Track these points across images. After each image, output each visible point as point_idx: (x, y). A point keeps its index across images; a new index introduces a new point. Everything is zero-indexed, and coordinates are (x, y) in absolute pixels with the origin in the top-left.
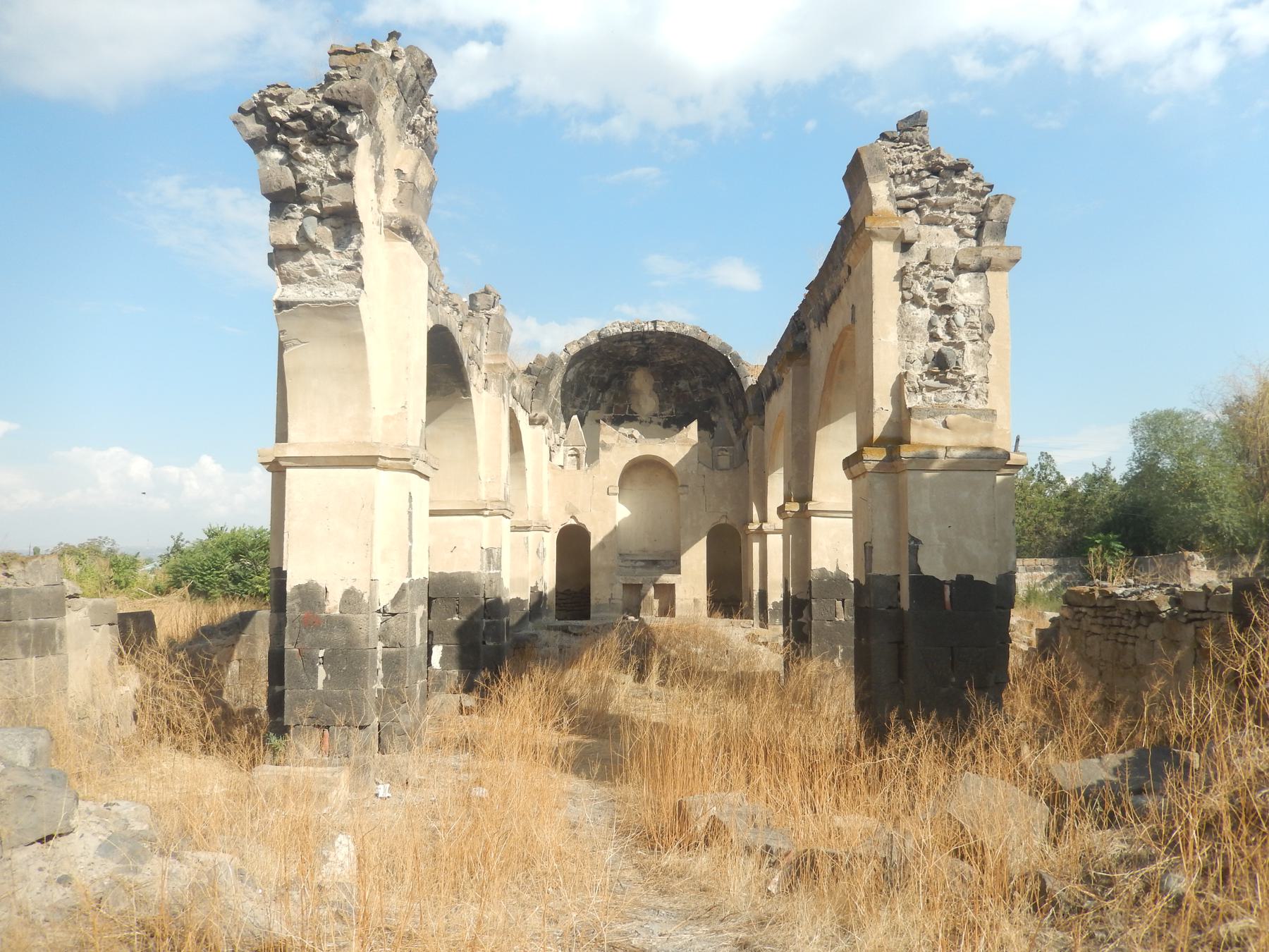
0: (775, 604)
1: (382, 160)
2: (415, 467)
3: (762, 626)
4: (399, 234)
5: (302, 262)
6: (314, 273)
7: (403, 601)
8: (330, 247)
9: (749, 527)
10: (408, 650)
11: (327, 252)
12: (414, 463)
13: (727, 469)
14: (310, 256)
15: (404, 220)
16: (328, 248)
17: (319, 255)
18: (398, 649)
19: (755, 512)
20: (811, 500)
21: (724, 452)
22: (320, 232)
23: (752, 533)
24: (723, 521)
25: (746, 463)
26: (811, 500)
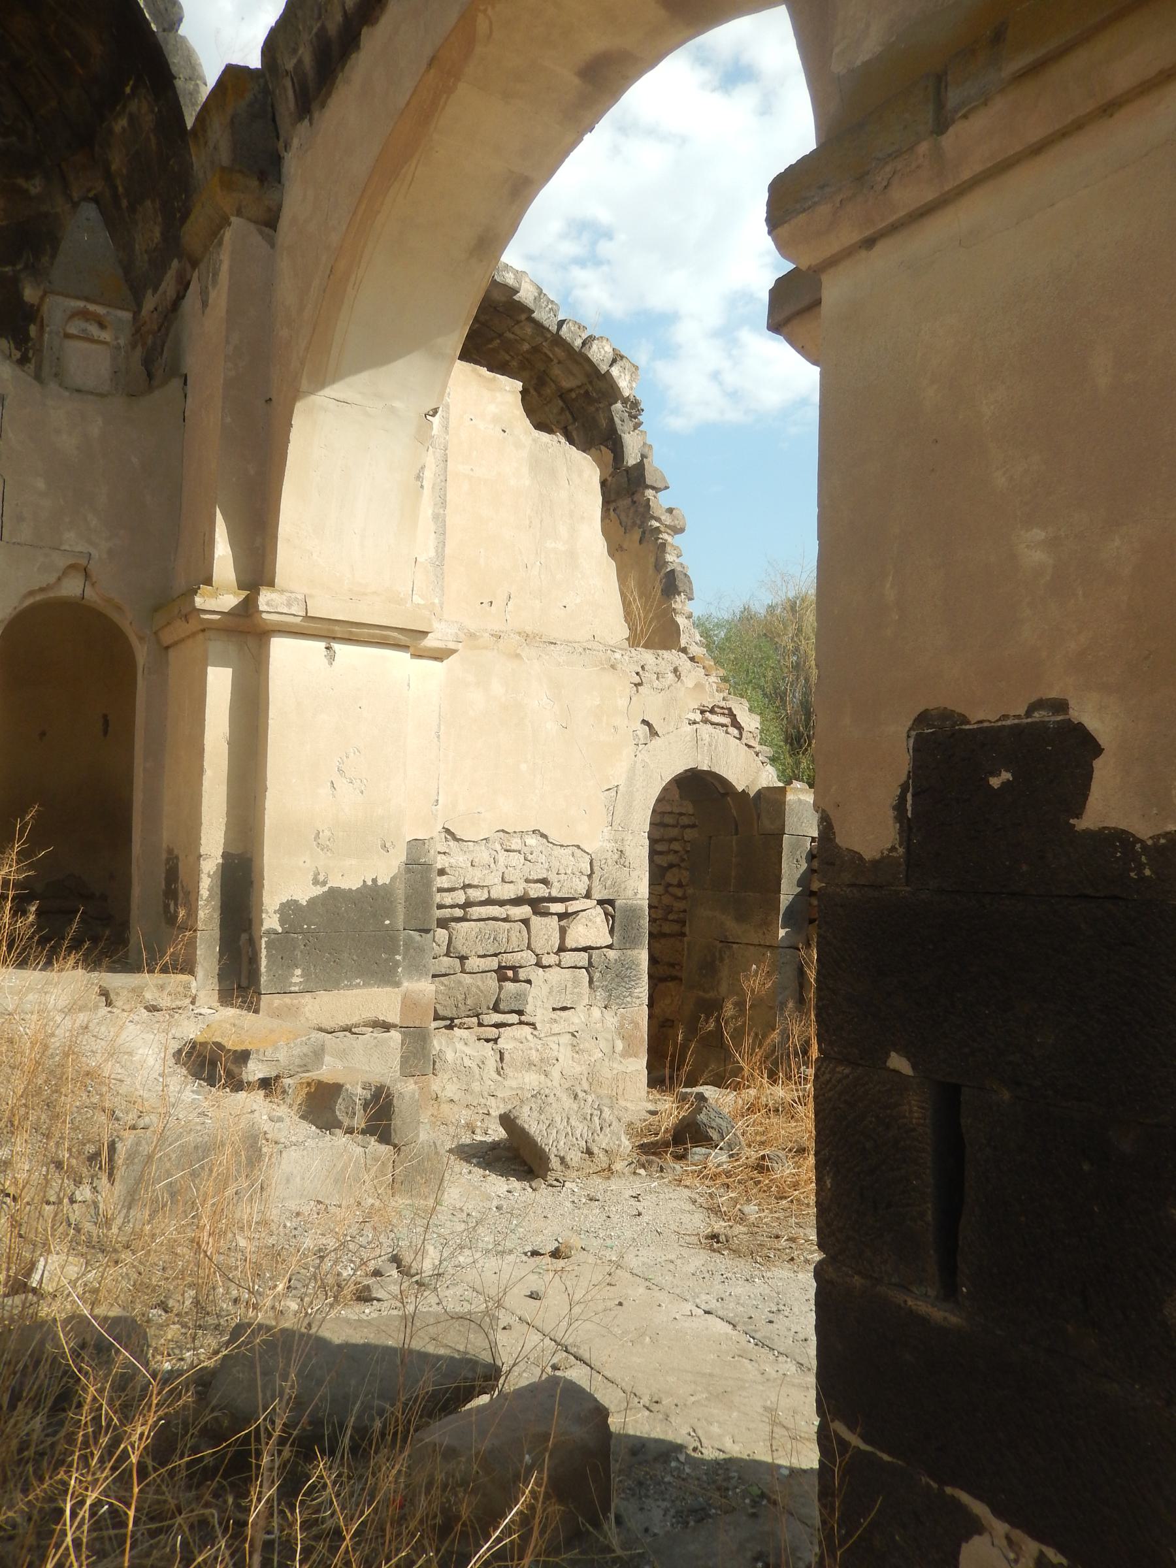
0: (289, 910)
3: (226, 998)
9: (199, 602)
13: (102, 395)
19: (223, 550)
20: (271, 584)
21: (94, 330)
23: (207, 628)
24: (72, 588)
25: (176, 383)
26: (271, 584)
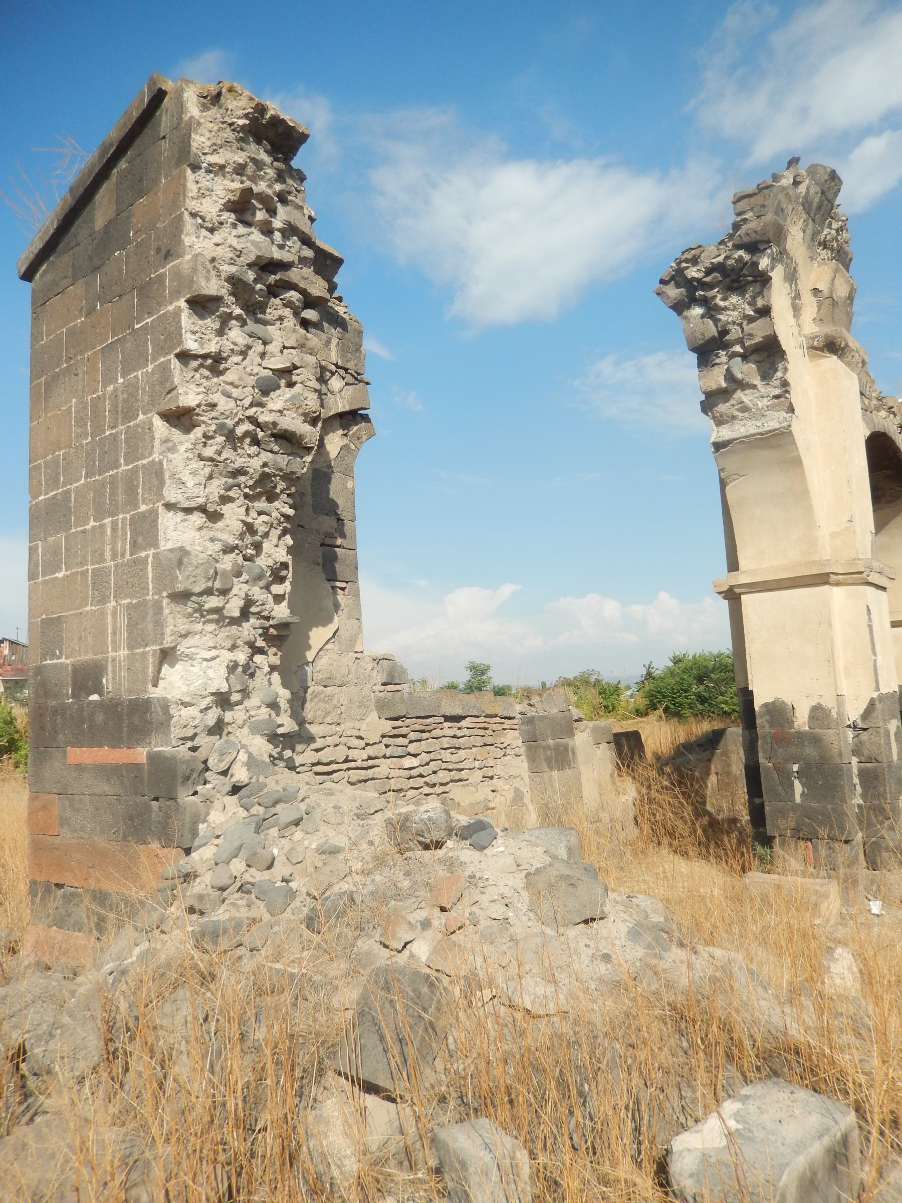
2: (870, 579)
4: (823, 351)
5: (732, 402)
6: (745, 409)
7: (873, 715)
8: (757, 381)
10: (885, 765)
11: (754, 387)
12: (868, 576)
14: (739, 394)
15: (826, 336)
16: (755, 383)
17: (747, 392)
18: (874, 765)
22: (746, 370)
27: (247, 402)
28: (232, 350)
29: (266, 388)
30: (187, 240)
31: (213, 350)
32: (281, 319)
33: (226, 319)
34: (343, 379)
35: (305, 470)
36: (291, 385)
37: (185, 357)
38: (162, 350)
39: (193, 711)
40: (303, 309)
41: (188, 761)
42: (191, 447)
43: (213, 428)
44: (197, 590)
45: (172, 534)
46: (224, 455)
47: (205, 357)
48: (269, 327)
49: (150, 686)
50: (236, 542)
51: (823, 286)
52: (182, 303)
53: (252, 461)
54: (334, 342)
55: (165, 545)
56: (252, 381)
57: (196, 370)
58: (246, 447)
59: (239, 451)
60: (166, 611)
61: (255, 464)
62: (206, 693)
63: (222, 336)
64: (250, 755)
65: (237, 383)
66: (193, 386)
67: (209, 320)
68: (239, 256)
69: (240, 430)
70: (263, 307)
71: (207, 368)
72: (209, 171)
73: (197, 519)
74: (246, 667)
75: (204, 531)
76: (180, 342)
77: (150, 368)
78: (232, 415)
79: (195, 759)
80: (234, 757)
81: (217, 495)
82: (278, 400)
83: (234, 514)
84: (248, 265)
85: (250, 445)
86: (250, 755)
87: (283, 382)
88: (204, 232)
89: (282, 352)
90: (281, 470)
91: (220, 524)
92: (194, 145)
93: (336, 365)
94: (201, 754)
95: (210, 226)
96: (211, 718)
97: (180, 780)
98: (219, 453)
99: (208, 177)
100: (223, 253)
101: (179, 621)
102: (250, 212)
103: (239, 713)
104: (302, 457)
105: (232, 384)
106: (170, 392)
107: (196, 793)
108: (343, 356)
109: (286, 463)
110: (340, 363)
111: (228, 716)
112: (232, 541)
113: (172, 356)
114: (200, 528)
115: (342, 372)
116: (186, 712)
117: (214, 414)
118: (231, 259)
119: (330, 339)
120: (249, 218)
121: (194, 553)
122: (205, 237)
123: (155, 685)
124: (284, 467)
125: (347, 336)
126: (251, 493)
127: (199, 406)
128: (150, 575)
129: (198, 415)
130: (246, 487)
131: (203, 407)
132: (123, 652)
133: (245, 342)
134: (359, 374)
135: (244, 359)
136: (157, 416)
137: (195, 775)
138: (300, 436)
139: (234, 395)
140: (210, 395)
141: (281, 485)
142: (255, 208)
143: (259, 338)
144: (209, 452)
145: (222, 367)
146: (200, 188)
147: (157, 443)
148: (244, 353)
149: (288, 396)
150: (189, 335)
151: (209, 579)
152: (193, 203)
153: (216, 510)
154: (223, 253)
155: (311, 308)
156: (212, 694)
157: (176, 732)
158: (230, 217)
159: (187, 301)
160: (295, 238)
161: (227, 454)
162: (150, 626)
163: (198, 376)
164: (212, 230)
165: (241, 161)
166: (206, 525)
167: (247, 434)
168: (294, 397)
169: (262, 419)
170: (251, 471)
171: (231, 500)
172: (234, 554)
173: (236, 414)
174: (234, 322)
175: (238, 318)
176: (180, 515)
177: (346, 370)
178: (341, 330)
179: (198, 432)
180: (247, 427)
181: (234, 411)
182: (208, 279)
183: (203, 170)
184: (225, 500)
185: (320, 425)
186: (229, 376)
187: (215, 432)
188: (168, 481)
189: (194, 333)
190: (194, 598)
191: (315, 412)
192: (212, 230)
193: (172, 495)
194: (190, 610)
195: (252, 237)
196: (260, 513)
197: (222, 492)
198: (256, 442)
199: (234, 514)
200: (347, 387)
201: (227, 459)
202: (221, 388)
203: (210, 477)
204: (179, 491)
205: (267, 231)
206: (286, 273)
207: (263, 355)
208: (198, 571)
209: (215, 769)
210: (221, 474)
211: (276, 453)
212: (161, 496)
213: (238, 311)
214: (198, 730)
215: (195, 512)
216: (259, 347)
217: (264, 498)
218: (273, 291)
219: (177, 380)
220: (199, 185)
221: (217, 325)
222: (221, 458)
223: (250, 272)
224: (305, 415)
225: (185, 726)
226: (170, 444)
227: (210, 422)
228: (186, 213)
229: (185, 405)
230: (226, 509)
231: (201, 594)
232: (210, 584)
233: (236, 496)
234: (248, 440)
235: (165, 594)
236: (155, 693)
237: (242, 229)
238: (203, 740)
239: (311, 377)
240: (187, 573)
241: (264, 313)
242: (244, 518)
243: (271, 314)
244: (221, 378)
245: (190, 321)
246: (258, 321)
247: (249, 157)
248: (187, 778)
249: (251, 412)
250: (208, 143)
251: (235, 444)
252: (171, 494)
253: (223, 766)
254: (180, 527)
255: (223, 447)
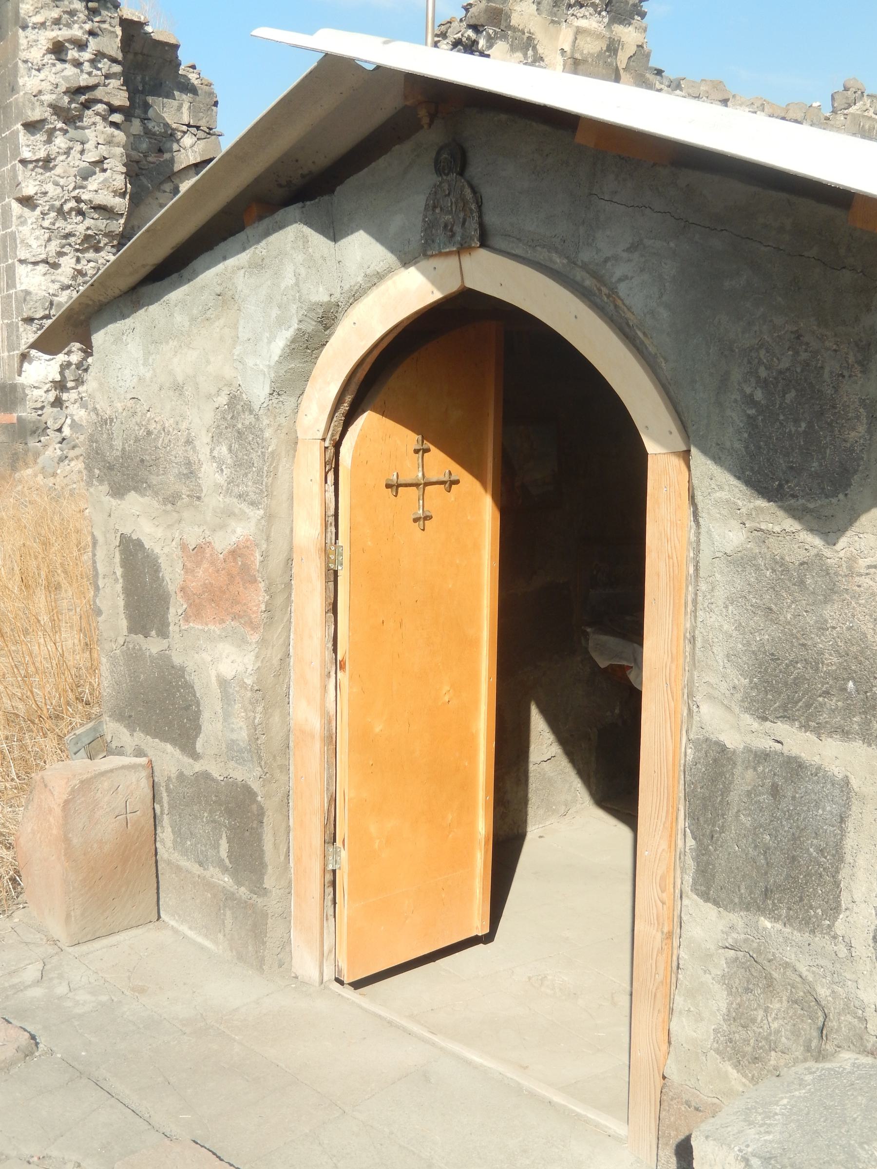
1: (534, 48)
27: (71, 187)
28: (58, 153)
29: (86, 175)
30: (21, 81)
31: (42, 156)
32: (94, 124)
33: (51, 133)
34: (195, 135)
35: (121, 229)
36: (104, 170)
37: (23, 162)
38: (14, 157)
39: (41, 392)
40: (110, 115)
41: (34, 422)
42: (35, 221)
43: (47, 208)
44: (38, 316)
45: (24, 280)
46: (57, 225)
47: (37, 161)
48: (86, 131)
49: (16, 376)
50: (70, 282)
51: (567, 48)
52: (19, 126)
53: (78, 226)
54: (186, 106)
55: (20, 287)
56: (74, 171)
57: (32, 170)
58: (74, 217)
59: (69, 220)
60: (21, 330)
61: (81, 229)
62: (47, 381)
63: (51, 143)
64: (73, 421)
65: (62, 175)
66: (31, 181)
67: (38, 135)
68: (56, 88)
69: (66, 208)
70: (80, 118)
71: (40, 167)
72: (34, 28)
73: (42, 268)
74: (79, 366)
75: (48, 276)
76: (19, 154)
77: (9, 166)
78: (58, 198)
79: (39, 421)
80: (63, 421)
81: (54, 251)
82: (93, 183)
83: (68, 263)
84: (63, 92)
85: (76, 216)
86: (73, 421)
87: (97, 169)
88: (34, 72)
89: (97, 147)
90: (101, 231)
91: (60, 271)
92: (22, 12)
93: (189, 125)
94: (43, 418)
95: (37, 68)
96: (52, 396)
97: (29, 433)
98: (54, 224)
99: (34, 32)
100: (46, 86)
101: (30, 335)
102: (64, 53)
103: (74, 394)
104: (117, 220)
105: (59, 176)
106: (18, 185)
107: (40, 441)
108: (195, 116)
109: (104, 225)
110: (192, 123)
111: (65, 396)
112: (67, 281)
113: (17, 162)
114: (45, 274)
115: (193, 130)
116: (37, 393)
117: (46, 199)
118: (51, 90)
119: (182, 104)
120: (63, 57)
121: (34, 292)
122: (34, 76)
123: (20, 375)
124: (103, 229)
125: (198, 99)
126: (81, 248)
127: (36, 194)
128: (14, 306)
129: (36, 200)
130: (76, 244)
131: (39, 195)
132: (6, 354)
133: (67, 146)
134: (210, 129)
135: (67, 158)
136: (13, 201)
137: (40, 431)
138: (111, 207)
139: (61, 184)
140: (44, 186)
141: (105, 240)
142: (68, 49)
143: (77, 141)
144: (46, 224)
145: (51, 165)
146: (28, 42)
147: (14, 219)
148: (67, 152)
149: (101, 179)
150: (24, 148)
151: (46, 309)
152: (24, 53)
153: (55, 262)
154: (46, 86)
155: (116, 112)
156: (51, 382)
157: (30, 404)
158: (50, 58)
159: (22, 125)
160: (106, 60)
161: (60, 223)
162: (15, 338)
163: (34, 174)
164: (39, 70)
165: (56, 16)
166: (49, 272)
167: (72, 209)
168: (105, 180)
169: (84, 197)
170: (78, 234)
171: (65, 254)
172: (69, 290)
173: (63, 197)
174: (58, 132)
175: (61, 130)
176: (30, 266)
177: (198, 128)
178: (191, 95)
179: (39, 209)
180: (72, 204)
181: (61, 195)
182: (33, 109)
183: (30, 28)
184: (61, 254)
185: (128, 197)
186: (58, 170)
187: (48, 210)
188: (19, 246)
189: (28, 146)
190: (36, 321)
191: (121, 189)
192: (39, 70)
193: (22, 255)
194: (35, 329)
195: (66, 73)
196: (89, 261)
197: (58, 249)
198: (80, 213)
199: (68, 263)
200: (198, 142)
201: (59, 228)
202: (52, 179)
203: (49, 240)
204: (27, 251)
205: (78, 64)
206: (93, 93)
207: (82, 152)
208: (37, 304)
209: (52, 427)
210: (56, 238)
211: (96, 219)
212: (16, 257)
213: (60, 125)
214: (45, 404)
215: (40, 264)
216: (78, 147)
217: (91, 251)
218: (87, 105)
219: (20, 178)
220: (28, 39)
221: (45, 138)
222: (56, 227)
223: (65, 97)
224: (115, 192)
225: (36, 401)
226: (23, 219)
227: (44, 204)
228: (19, 61)
229: (27, 194)
230: (63, 260)
231: (42, 318)
232: (47, 312)
233: (68, 252)
234: (74, 213)
235: (20, 319)
236: (20, 380)
237: (59, 66)
238: (48, 410)
239: (118, 164)
240: (29, 306)
241: (82, 121)
242: (74, 267)
243: (86, 121)
244: (52, 172)
245: (25, 138)
246: (77, 128)
247: (63, 11)
248: (34, 432)
249: (75, 193)
250: (32, 8)
251: (65, 216)
252: (22, 254)
253: (57, 426)
254: (30, 274)
255: (56, 220)
